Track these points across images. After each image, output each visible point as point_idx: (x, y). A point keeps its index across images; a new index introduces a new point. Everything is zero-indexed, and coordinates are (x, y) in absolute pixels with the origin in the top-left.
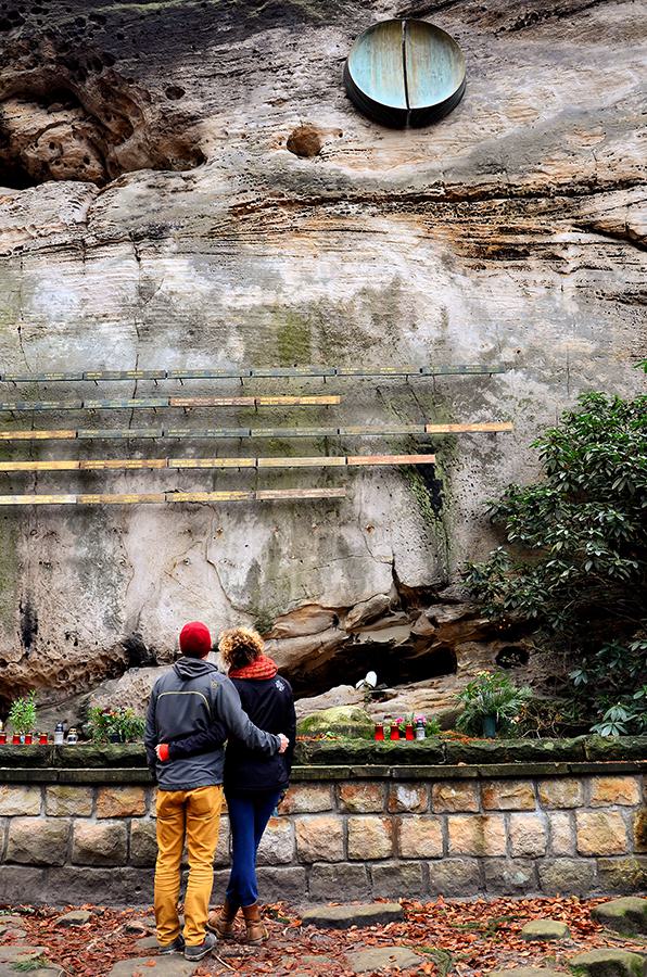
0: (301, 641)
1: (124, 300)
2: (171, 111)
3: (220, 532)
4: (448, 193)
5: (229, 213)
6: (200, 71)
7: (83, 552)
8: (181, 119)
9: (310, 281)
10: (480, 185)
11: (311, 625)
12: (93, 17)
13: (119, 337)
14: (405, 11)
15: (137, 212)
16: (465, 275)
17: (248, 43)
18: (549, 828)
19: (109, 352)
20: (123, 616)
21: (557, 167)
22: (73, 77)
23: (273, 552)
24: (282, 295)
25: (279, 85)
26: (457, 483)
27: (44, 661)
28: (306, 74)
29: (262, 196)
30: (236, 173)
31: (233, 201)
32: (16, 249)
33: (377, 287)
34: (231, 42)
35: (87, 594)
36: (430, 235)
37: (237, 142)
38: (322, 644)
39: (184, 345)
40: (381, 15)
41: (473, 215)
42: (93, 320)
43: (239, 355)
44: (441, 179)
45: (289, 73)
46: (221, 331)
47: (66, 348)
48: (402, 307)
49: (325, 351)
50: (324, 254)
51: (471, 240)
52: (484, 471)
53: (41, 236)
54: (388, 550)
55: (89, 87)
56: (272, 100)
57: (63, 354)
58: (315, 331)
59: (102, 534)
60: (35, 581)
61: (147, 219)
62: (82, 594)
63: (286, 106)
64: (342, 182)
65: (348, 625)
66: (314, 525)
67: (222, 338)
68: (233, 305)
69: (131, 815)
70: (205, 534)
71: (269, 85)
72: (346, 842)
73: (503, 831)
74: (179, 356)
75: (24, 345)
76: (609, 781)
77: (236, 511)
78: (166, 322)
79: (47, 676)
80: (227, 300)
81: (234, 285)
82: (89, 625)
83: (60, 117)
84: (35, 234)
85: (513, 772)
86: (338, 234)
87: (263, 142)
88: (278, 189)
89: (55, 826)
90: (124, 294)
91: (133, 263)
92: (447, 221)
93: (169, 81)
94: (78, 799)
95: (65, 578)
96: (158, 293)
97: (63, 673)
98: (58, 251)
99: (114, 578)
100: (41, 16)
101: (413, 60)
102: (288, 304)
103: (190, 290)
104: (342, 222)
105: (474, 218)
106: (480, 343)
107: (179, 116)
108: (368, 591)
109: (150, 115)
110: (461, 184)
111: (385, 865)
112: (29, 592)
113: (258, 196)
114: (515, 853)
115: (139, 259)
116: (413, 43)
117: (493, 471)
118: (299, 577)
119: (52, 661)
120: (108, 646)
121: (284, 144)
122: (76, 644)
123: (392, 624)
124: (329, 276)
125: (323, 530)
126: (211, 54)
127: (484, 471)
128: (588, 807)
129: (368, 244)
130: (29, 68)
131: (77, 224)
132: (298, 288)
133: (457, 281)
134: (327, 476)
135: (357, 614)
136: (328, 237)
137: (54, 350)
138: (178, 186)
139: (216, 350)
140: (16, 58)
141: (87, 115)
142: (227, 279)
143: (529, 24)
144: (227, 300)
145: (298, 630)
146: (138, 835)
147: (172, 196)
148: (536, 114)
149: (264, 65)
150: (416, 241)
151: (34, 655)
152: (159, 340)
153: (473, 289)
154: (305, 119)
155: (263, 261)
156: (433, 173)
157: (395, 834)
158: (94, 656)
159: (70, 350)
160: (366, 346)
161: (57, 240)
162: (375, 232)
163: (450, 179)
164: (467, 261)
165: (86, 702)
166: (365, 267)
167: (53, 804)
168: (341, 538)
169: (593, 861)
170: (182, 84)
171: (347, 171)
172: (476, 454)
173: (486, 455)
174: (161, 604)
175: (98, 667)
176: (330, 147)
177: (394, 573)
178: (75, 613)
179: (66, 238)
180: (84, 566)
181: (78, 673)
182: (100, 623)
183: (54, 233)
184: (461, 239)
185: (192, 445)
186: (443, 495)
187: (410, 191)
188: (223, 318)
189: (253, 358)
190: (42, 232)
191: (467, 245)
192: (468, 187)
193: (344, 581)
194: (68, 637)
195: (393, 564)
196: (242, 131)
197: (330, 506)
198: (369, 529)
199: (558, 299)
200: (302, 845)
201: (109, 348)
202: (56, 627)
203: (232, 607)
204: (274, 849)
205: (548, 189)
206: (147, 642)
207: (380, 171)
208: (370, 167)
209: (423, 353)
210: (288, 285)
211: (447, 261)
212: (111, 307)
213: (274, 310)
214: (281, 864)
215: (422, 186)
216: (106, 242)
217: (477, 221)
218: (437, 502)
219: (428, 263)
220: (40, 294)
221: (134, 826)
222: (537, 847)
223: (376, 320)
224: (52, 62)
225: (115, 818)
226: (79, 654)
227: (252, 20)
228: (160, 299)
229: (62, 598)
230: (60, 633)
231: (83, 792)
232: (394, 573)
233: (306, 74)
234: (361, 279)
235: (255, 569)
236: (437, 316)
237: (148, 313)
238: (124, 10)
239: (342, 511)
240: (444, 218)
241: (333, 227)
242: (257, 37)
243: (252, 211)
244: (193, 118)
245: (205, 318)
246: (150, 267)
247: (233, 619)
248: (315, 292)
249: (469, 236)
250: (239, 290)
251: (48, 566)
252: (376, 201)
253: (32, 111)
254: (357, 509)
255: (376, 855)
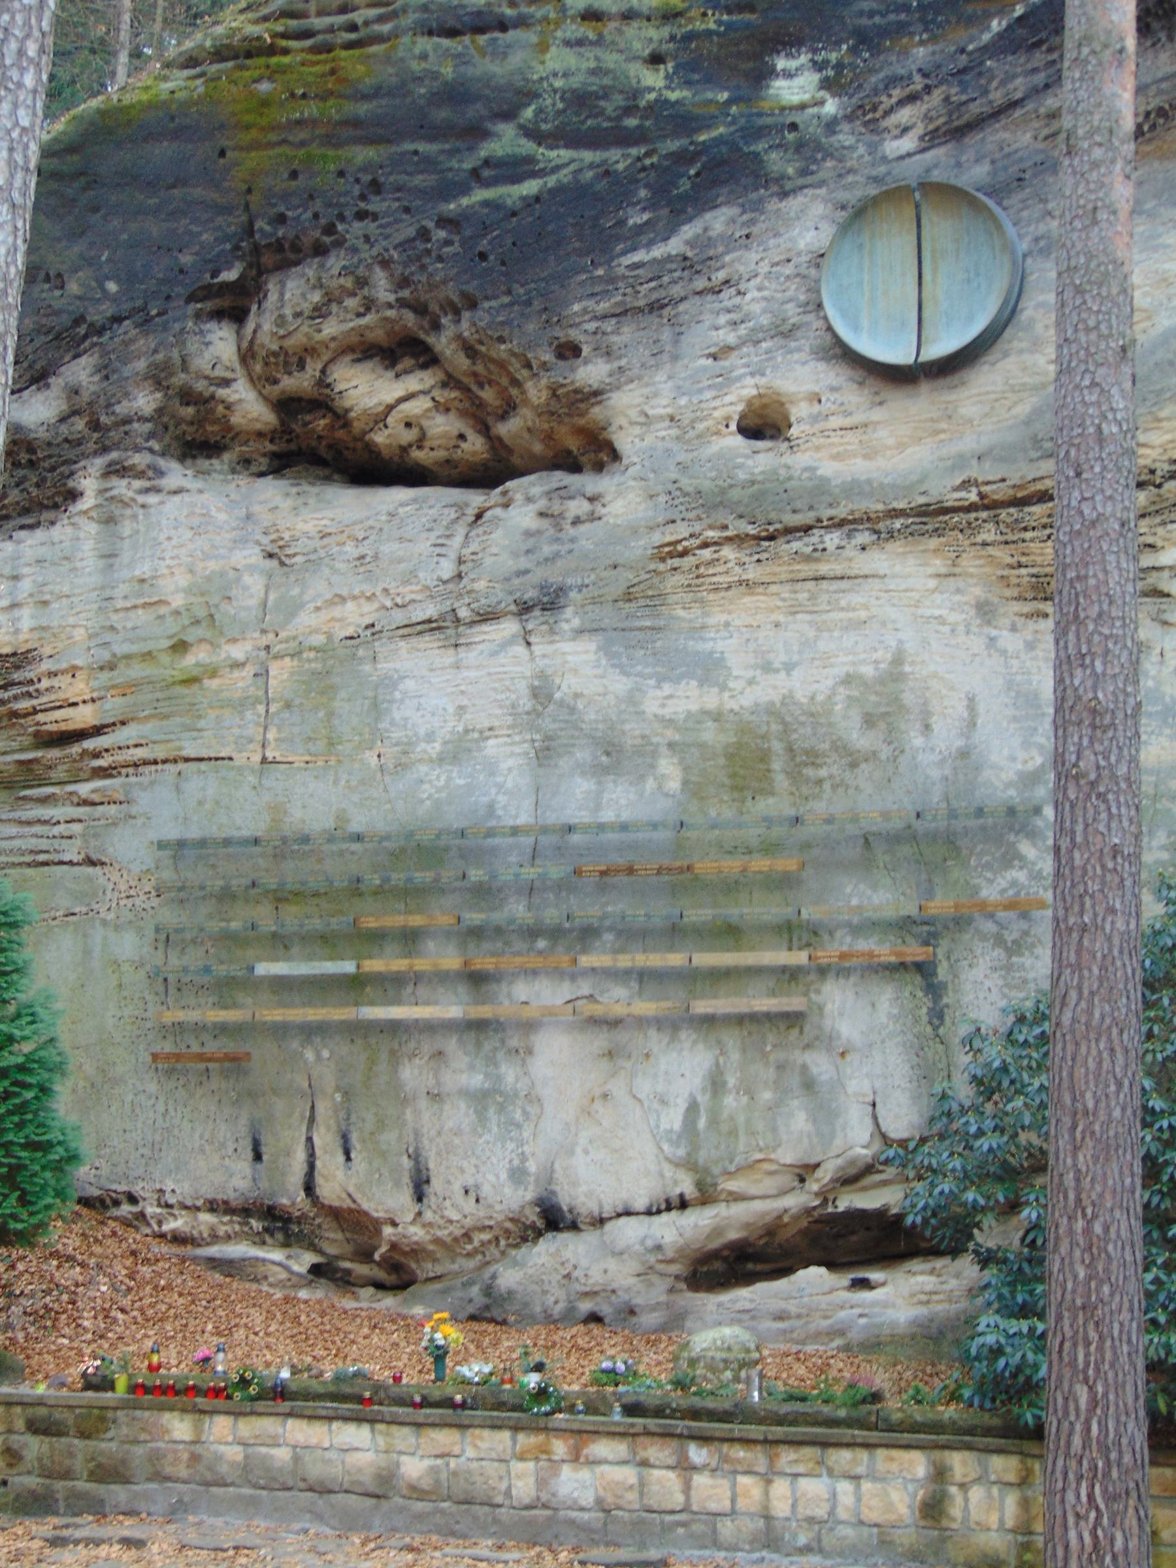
0: (758, 1206)
1: (513, 706)
2: (563, 386)
3: (647, 1055)
4: (982, 496)
5: (652, 558)
6: (604, 306)
7: (476, 1080)
8: (579, 396)
9: (768, 668)
10: (1034, 480)
11: (769, 1185)
12: (443, 222)
13: (511, 762)
14: (937, 129)
15: (524, 563)
16: (1014, 629)
17: (675, 245)
18: (834, 1495)
19: (500, 787)
20: (532, 1166)
21: (1168, 432)
22: (422, 328)
23: (716, 1084)
24: (726, 694)
25: (723, 319)
26: (968, 987)
27: (441, 1222)
28: (766, 293)
29: (697, 528)
30: (660, 488)
31: (658, 538)
32: (367, 627)
33: (868, 671)
34: (650, 244)
35: (486, 1137)
36: (957, 570)
37: (664, 431)
38: (786, 1211)
39: (599, 771)
40: (895, 144)
41: (1025, 529)
42: (476, 735)
43: (674, 785)
44: (974, 472)
45: (739, 293)
46: (646, 752)
47: (442, 783)
48: (908, 698)
49: (795, 776)
50: (790, 618)
51: (1023, 571)
52: (1009, 968)
53: (397, 605)
54: (866, 1086)
55: (443, 343)
56: (713, 350)
57: (439, 790)
58: (777, 746)
59: (500, 1055)
60: (423, 1117)
61: (539, 575)
62: (480, 1136)
63: (733, 360)
64: (821, 488)
65: (815, 1187)
66: (769, 1048)
67: (649, 760)
68: (660, 712)
69: (448, 1455)
70: (630, 1056)
71: (708, 319)
72: (641, 1494)
73: (789, 1494)
74: (593, 787)
75: (387, 779)
76: (895, 1453)
77: (670, 1025)
78: (572, 737)
79: (448, 1240)
80: (651, 706)
81: (661, 680)
82: (491, 1177)
83: (414, 382)
84: (389, 604)
85: (800, 1438)
86: (810, 585)
87: (700, 426)
88: (722, 517)
89: (382, 1460)
90: (514, 697)
91: (520, 650)
92: (985, 544)
93: (558, 332)
94: (404, 1437)
95: (459, 1114)
96: (558, 695)
97: (467, 1236)
98: (420, 633)
99: (518, 1116)
100: (371, 227)
101: (934, 251)
102: (736, 708)
103: (601, 690)
104: (814, 566)
105: (1029, 535)
106: (1021, 755)
107: (576, 391)
108: (838, 1143)
109: (536, 392)
110: (1003, 480)
111: (677, 1517)
112: (417, 1134)
113: (691, 530)
114: (799, 1516)
115: (529, 644)
116: (935, 219)
117: (1022, 967)
118: (748, 1121)
119: (451, 1222)
120: (515, 1206)
121: (733, 427)
122: (477, 1201)
123: (885, 1183)
124: (796, 658)
125: (781, 1055)
126: (621, 271)
127: (1009, 968)
128: (872, 1476)
129: (856, 599)
130: (359, 315)
131: (445, 582)
132: (751, 682)
133: (1001, 643)
134: (790, 975)
135: (826, 1174)
136: (795, 592)
137: (426, 786)
138: (579, 512)
139: (642, 778)
140: (340, 302)
141: (450, 381)
142: (648, 670)
143: (1153, 127)
144: (651, 706)
145: (753, 1190)
146: (455, 1474)
147: (571, 531)
148: (1149, 318)
149: (700, 283)
150: (932, 583)
151: (428, 1216)
152: (564, 763)
153: (1023, 656)
154: (762, 381)
155: (701, 638)
156: (961, 461)
157: (687, 1489)
158: (500, 1217)
159: (447, 786)
160: (853, 765)
161: (419, 614)
162: (866, 577)
163: (987, 472)
164: (1017, 607)
165: (494, 1277)
166: (849, 640)
167: (381, 1441)
168: (804, 1068)
169: (875, 1530)
170: (574, 335)
171: (828, 469)
172: (999, 941)
173: (1014, 942)
174: (579, 1150)
175: (507, 1232)
176: (803, 427)
177: (875, 1118)
178: (474, 1161)
179: (430, 610)
180: (480, 1099)
181: (486, 1236)
182: (504, 1176)
183: (414, 601)
184: (1006, 572)
185: (610, 929)
186: (947, 1006)
187: (922, 500)
188: (647, 732)
189: (694, 789)
190: (399, 600)
191: (1014, 581)
192: (1014, 486)
193: (809, 1127)
194: (466, 1192)
195: (874, 1105)
196: (669, 410)
197: (793, 1020)
198: (843, 1054)
199: (1153, 673)
200: (601, 1493)
201: (500, 779)
202: (452, 1179)
203: (667, 1159)
204: (576, 1494)
205: (1152, 472)
206: (564, 1202)
207: (880, 462)
208: (866, 457)
209: (935, 774)
210: (737, 677)
211: (985, 611)
212: (497, 716)
213: (717, 717)
214: (582, 1509)
215: (943, 490)
216: (487, 617)
217: (1032, 540)
218: (937, 1016)
219: (953, 617)
220: (402, 701)
221: (453, 1465)
222: (821, 1512)
223: (869, 721)
224: (390, 306)
225: (437, 1456)
226: (482, 1214)
227: (680, 197)
228: (561, 703)
229: (457, 1141)
230: (457, 1187)
231: (406, 1430)
232: (875, 1118)
233: (766, 293)
234: (840, 659)
235: (693, 1108)
236: (961, 710)
237: (548, 725)
238: (486, 203)
239: (807, 1028)
240: (979, 539)
241: (802, 575)
242: (689, 231)
243: (684, 553)
244: (596, 393)
245: (623, 732)
246: (544, 656)
247: (668, 1174)
248: (775, 687)
249: (1020, 566)
250: (667, 688)
251: (435, 1097)
252: (867, 520)
253: (374, 376)
254: (827, 1023)
255: (669, 1507)
